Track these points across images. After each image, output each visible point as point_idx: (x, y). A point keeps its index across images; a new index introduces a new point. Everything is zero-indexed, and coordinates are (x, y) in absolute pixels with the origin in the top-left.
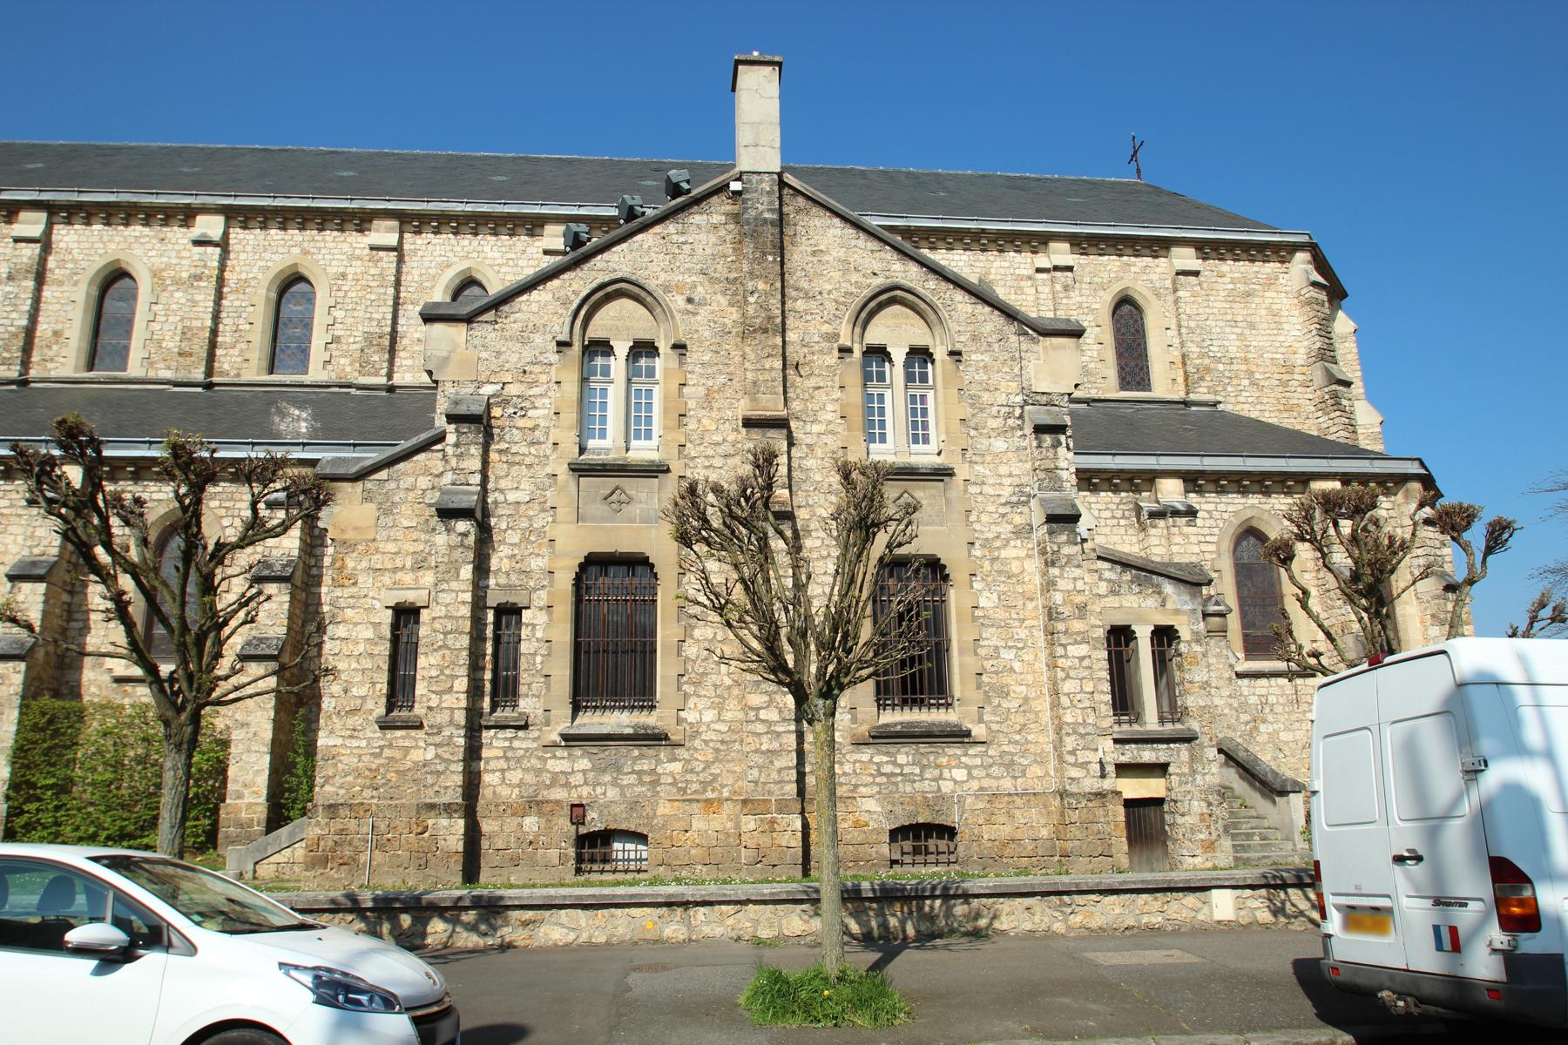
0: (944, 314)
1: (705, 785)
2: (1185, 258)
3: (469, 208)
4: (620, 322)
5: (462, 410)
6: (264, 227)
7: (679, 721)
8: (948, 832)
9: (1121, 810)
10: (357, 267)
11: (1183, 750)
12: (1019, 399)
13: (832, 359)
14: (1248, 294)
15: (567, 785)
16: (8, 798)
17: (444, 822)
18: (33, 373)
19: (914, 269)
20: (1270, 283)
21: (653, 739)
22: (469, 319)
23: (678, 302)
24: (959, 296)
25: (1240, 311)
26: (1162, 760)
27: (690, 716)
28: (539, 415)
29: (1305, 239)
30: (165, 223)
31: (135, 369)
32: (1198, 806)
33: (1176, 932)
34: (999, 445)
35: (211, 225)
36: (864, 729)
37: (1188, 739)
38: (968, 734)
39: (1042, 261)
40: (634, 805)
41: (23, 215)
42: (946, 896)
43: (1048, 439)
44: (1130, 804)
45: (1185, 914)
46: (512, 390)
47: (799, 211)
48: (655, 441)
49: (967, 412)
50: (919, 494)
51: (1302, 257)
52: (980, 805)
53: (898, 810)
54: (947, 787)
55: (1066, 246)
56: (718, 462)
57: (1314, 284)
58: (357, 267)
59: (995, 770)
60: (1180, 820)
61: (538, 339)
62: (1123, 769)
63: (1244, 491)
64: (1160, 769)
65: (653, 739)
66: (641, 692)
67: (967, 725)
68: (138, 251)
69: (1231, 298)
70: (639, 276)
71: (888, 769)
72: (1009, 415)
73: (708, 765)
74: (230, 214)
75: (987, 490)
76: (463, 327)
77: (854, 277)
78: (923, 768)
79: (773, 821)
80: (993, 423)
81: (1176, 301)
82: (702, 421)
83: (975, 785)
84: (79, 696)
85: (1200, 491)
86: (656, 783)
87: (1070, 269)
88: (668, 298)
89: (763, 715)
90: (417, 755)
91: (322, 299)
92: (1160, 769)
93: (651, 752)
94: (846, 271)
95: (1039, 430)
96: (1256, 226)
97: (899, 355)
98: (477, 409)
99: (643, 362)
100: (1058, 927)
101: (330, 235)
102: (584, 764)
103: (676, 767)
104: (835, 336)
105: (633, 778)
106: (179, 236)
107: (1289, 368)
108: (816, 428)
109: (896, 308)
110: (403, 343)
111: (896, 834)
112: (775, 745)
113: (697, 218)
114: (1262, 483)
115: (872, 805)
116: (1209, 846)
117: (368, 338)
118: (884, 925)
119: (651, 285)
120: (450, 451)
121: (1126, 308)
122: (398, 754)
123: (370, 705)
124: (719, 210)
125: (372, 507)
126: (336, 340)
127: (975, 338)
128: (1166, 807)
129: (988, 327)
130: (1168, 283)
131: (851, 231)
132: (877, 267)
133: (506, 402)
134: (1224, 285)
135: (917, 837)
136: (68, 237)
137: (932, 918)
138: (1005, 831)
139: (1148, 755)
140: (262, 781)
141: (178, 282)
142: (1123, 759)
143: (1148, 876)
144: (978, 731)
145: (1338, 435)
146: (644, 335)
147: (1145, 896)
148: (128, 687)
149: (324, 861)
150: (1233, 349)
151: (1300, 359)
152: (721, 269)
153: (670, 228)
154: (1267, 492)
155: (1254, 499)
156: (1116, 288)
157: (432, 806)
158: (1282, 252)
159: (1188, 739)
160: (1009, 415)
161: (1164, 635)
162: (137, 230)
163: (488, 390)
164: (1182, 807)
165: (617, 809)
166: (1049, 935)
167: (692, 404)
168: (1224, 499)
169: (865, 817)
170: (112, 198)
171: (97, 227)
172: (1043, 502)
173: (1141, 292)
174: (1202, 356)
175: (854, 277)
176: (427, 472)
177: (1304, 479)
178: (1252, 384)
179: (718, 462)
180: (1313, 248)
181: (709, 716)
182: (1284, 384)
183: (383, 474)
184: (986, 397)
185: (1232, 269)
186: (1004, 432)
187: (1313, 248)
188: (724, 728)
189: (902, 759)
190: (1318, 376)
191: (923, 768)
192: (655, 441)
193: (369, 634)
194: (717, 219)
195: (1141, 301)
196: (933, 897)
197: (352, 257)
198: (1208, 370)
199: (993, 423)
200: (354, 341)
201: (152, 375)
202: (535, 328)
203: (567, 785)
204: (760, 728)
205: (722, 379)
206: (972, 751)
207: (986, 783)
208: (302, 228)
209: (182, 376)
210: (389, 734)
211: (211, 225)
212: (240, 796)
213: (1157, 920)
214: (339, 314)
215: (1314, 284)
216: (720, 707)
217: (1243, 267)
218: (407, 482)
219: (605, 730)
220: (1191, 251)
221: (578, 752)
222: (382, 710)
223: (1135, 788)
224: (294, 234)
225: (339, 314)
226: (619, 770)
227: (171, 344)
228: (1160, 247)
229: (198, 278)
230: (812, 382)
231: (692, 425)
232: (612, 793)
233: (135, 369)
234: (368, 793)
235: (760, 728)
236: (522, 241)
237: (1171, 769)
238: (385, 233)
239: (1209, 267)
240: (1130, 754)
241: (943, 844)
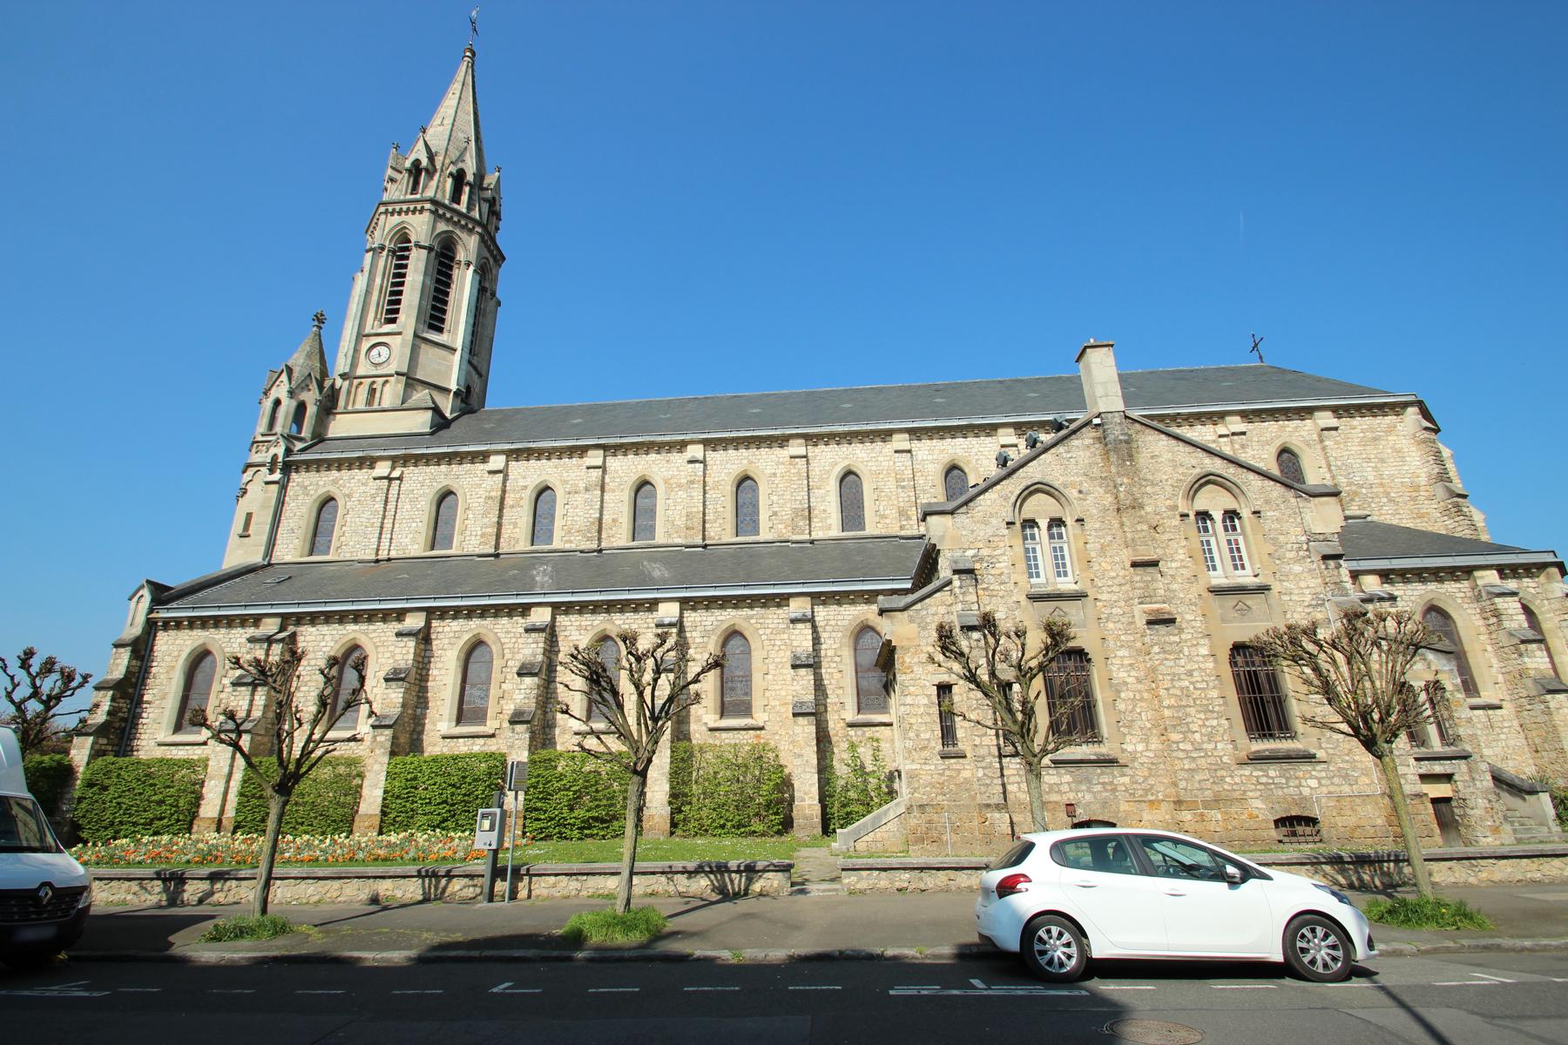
0: (1244, 488)
1: (1146, 791)
2: (1326, 419)
3: (846, 429)
4: (1040, 508)
5: (961, 567)
6: (725, 449)
7: (1124, 751)
8: (1311, 821)
9: (1430, 806)
10: (782, 469)
11: (1462, 764)
12: (1304, 538)
13: (1176, 521)
14: (1375, 439)
15: (1059, 791)
16: (670, 803)
17: (997, 815)
18: (603, 545)
19: (1218, 461)
20: (1390, 430)
21: (1109, 762)
22: (952, 513)
23: (1072, 493)
24: (1251, 476)
25: (1371, 451)
26: (1449, 771)
27: (1130, 748)
28: (1003, 566)
29: (1412, 398)
30: (669, 451)
31: (660, 538)
32: (1482, 803)
33: (1552, 883)
34: (1297, 568)
35: (696, 451)
36: (1243, 754)
37: (1465, 757)
38: (1314, 756)
39: (1221, 429)
40: (1105, 804)
41: (590, 453)
42: (1397, 861)
43: (1332, 563)
44: (1435, 801)
45: (1555, 872)
46: (985, 552)
47: (1137, 432)
48: (1070, 578)
49: (1271, 549)
50: (1249, 603)
51: (1412, 412)
52: (1332, 804)
53: (1277, 807)
54: (1306, 792)
55: (1238, 418)
56: (1116, 589)
57: (1426, 429)
58: (782, 469)
59: (1336, 780)
60: (1469, 811)
61: (994, 521)
62: (1425, 778)
63: (1423, 581)
64: (1448, 778)
65: (1109, 762)
66: (745, 709)
67: (1313, 751)
68: (655, 469)
69: (1363, 442)
70: (1047, 480)
71: (1264, 780)
72: (1300, 549)
73: (1146, 778)
74: (706, 443)
75: (1295, 598)
76: (949, 517)
77: (1181, 470)
78: (1288, 779)
79: (1202, 815)
80: (1292, 555)
81: (1324, 448)
82: (1101, 564)
83: (1324, 790)
84: (689, 740)
85: (1391, 582)
86: (1114, 790)
87: (1244, 433)
88: (1066, 491)
89: (1181, 746)
90: (966, 774)
91: (763, 490)
92: (1448, 778)
93: (1107, 770)
94: (1175, 467)
95: (1325, 558)
96: (1372, 392)
97: (1218, 516)
98: (968, 566)
99: (1055, 530)
100: (1472, 880)
101: (764, 451)
102: (1067, 778)
103: (1126, 780)
104: (1175, 507)
105: (1099, 788)
106: (678, 459)
107: (1417, 488)
108: (1174, 565)
109: (1210, 487)
110: (815, 513)
111: (1280, 822)
112: (1193, 766)
113: (1075, 442)
114: (1437, 574)
115: (1258, 804)
116: (1496, 830)
117: (795, 511)
118: (1360, 879)
119: (1056, 484)
120: (957, 591)
121: (1285, 456)
122: (954, 774)
123: (933, 744)
124: (1088, 436)
125: (915, 626)
126: (775, 514)
127: (1267, 502)
128: (1454, 804)
129: (1275, 494)
130: (1315, 436)
131: (1174, 442)
132: (1194, 462)
133: (981, 560)
134: (1357, 434)
135: (1292, 825)
136: (616, 463)
137: (1388, 874)
138: (1352, 821)
139: (1438, 768)
140: (815, 790)
141: (680, 486)
142: (1422, 771)
143: (1452, 850)
144: (1320, 754)
145: (1467, 533)
146: (1057, 515)
147: (1525, 860)
148: (717, 734)
149: (922, 840)
150: (1371, 478)
151: (1423, 480)
152: (1096, 472)
153: (1060, 449)
154: (1441, 580)
155: (1432, 586)
156: (1278, 444)
157: (988, 806)
158: (1397, 408)
159: (1465, 757)
160: (1300, 549)
161: (1435, 687)
162: (653, 456)
163: (970, 553)
164: (1471, 803)
165: (1094, 807)
166: (1468, 886)
167: (1093, 554)
168: (1409, 586)
169: (1256, 812)
170: (640, 439)
171: (631, 456)
172: (1338, 604)
173: (1295, 443)
174: (1350, 484)
175: (1181, 470)
176: (943, 604)
177: (1468, 571)
178: (1390, 501)
179: (1116, 589)
180: (1420, 405)
181: (1140, 747)
182: (1414, 499)
183: (918, 606)
184: (1282, 538)
185: (1361, 423)
186: (1298, 560)
187: (1420, 405)
188: (1151, 755)
189: (1272, 773)
190: (1440, 491)
191: (1288, 779)
192: (1070, 578)
193: (926, 701)
194: (1087, 442)
195: (1296, 450)
196: (1389, 861)
197: (778, 463)
198: (1356, 493)
199: (1292, 555)
200: (786, 513)
201: (670, 542)
202: (991, 515)
203: (1059, 791)
204: (1181, 755)
205: (1109, 538)
206: (1319, 767)
207: (1332, 789)
208: (747, 448)
209: (689, 542)
210: (947, 761)
211: (696, 451)
212: (803, 800)
213: (1538, 876)
214: (775, 498)
215: (1426, 429)
216: (1146, 741)
217: (1368, 420)
218: (932, 610)
219: (1079, 757)
220: (1329, 414)
221: (1062, 771)
222: (938, 746)
223: (1442, 790)
224: (743, 452)
225: (775, 498)
226: (1090, 782)
227: (681, 522)
228: (1305, 413)
229: (692, 482)
230: (1166, 536)
231: (1096, 567)
232: (1088, 797)
233: (660, 538)
234: (940, 798)
235: (1181, 755)
236: (879, 445)
237: (1456, 777)
238: (797, 447)
239: (1343, 423)
240: (1426, 767)
241: (1308, 830)
